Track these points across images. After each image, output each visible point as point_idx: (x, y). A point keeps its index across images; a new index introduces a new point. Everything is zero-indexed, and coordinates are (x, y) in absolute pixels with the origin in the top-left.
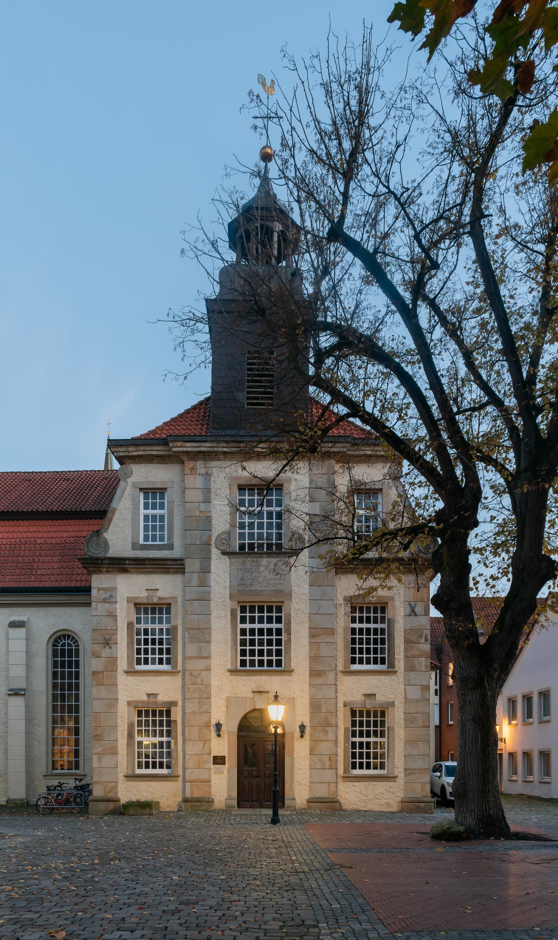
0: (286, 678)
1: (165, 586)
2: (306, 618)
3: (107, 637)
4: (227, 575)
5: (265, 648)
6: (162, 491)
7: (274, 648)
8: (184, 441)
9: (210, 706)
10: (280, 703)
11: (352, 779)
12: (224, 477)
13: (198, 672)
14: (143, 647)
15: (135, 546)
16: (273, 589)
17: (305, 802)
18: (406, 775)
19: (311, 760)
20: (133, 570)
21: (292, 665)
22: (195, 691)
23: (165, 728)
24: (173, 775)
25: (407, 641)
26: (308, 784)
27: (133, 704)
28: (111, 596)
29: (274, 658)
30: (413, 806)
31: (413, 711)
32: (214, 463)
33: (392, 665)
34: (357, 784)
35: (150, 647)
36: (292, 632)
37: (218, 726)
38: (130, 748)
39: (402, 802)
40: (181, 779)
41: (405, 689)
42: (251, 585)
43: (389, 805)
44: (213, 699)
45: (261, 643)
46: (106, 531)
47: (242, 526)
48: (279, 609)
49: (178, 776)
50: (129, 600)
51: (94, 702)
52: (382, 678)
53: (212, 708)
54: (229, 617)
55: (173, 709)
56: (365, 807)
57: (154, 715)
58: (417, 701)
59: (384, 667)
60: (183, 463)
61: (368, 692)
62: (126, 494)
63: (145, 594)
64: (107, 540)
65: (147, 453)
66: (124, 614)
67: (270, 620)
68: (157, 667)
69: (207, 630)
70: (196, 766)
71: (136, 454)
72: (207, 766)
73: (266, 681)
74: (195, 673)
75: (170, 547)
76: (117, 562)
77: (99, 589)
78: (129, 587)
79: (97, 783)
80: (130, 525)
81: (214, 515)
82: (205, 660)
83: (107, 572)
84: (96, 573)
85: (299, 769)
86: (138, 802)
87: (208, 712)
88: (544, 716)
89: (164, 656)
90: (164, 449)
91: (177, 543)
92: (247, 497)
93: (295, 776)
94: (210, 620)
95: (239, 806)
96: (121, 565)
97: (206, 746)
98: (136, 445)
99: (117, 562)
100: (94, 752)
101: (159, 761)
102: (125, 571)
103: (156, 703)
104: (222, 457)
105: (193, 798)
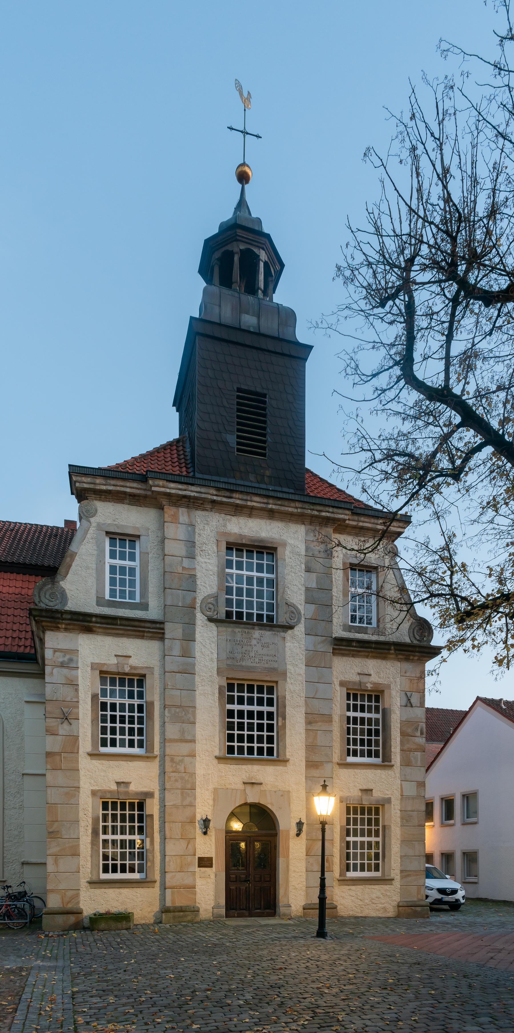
0: (280, 768)
1: (139, 653)
2: (302, 701)
3: (65, 710)
4: (214, 646)
5: (255, 733)
6: (133, 539)
7: (265, 733)
8: (167, 481)
9: (195, 799)
10: (329, 795)
11: (349, 883)
12: (212, 528)
13: (180, 758)
14: (109, 725)
15: (100, 601)
16: (266, 666)
17: (301, 909)
18: (402, 878)
19: (308, 862)
20: (100, 630)
21: (287, 754)
22: (176, 781)
23: (136, 824)
24: (148, 880)
25: (403, 734)
26: (304, 888)
27: (99, 794)
28: (71, 660)
29: (265, 745)
30: (410, 911)
31: (409, 808)
32: (199, 513)
33: (387, 758)
34: (353, 888)
35: (118, 725)
36: (287, 716)
37: (206, 822)
38: (95, 847)
39: (399, 906)
40: (158, 884)
41: (401, 785)
42: (242, 659)
43: (385, 909)
44: (198, 790)
45: (251, 728)
46: (63, 580)
47: (229, 591)
48: (271, 690)
49: (155, 882)
50: (93, 666)
51: (49, 790)
52: (379, 772)
53: (197, 801)
54: (217, 695)
55: (148, 802)
56: (362, 912)
57: (123, 808)
58: (413, 798)
59: (378, 761)
60: (161, 508)
61: (365, 787)
62: (88, 536)
63: (114, 661)
64: (64, 591)
65: (118, 488)
66: (87, 685)
67: (260, 702)
68: (127, 750)
69: (191, 709)
70: (178, 869)
71: (104, 488)
72: (191, 869)
73: (258, 771)
74: (177, 759)
75: (144, 606)
76: (81, 618)
77: (55, 650)
78: (95, 651)
79: (52, 891)
80: (95, 575)
81: (199, 575)
82: (190, 744)
83: (66, 630)
84: (52, 630)
85: (294, 871)
86: (108, 913)
87: (192, 805)
88: (467, 817)
89: (136, 738)
90: (140, 486)
91: (154, 602)
92: (234, 558)
93: (290, 879)
94: (194, 697)
95: (227, 916)
96: (84, 622)
97: (190, 846)
98: (106, 477)
99: (81, 618)
100: (49, 852)
101: (123, 863)
102: (89, 630)
103: (127, 793)
104: (208, 506)
105: (175, 907)
